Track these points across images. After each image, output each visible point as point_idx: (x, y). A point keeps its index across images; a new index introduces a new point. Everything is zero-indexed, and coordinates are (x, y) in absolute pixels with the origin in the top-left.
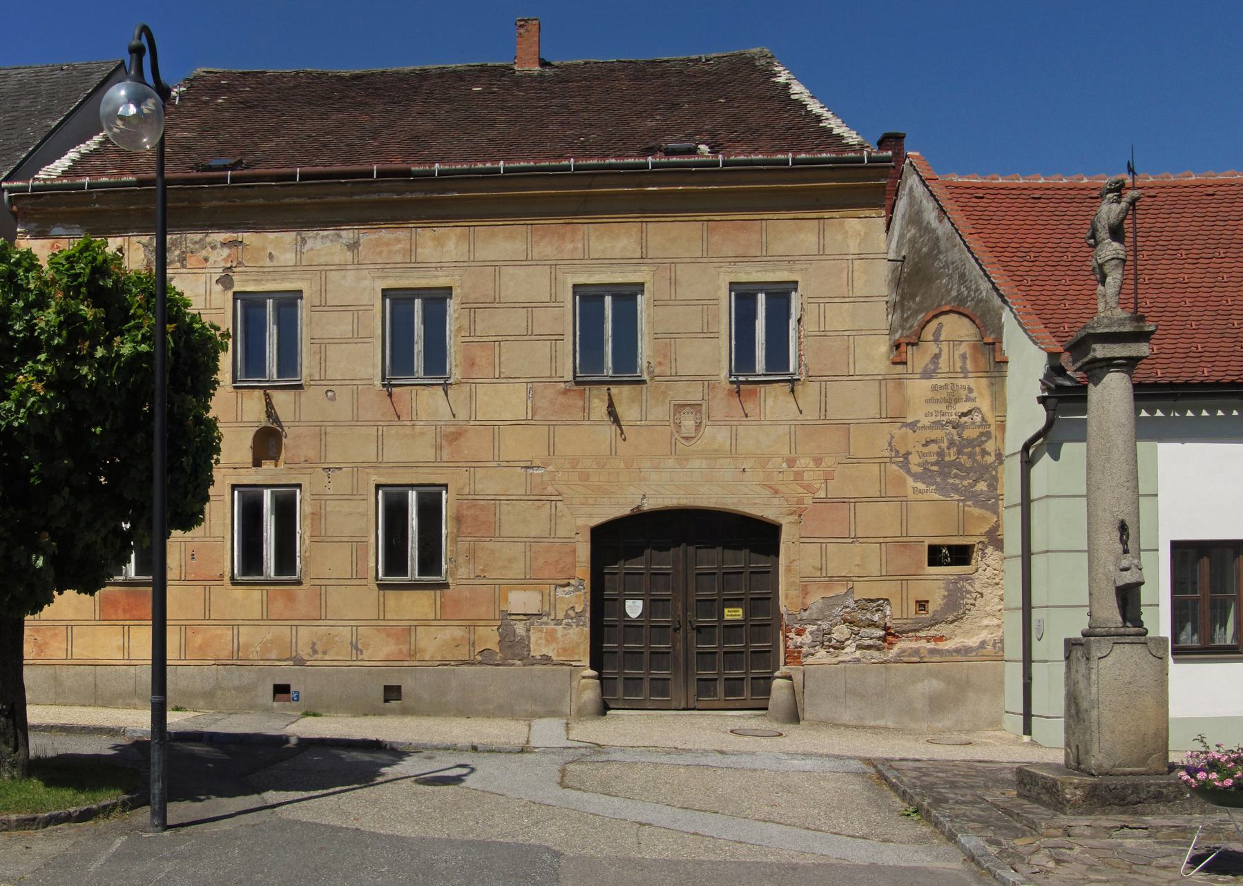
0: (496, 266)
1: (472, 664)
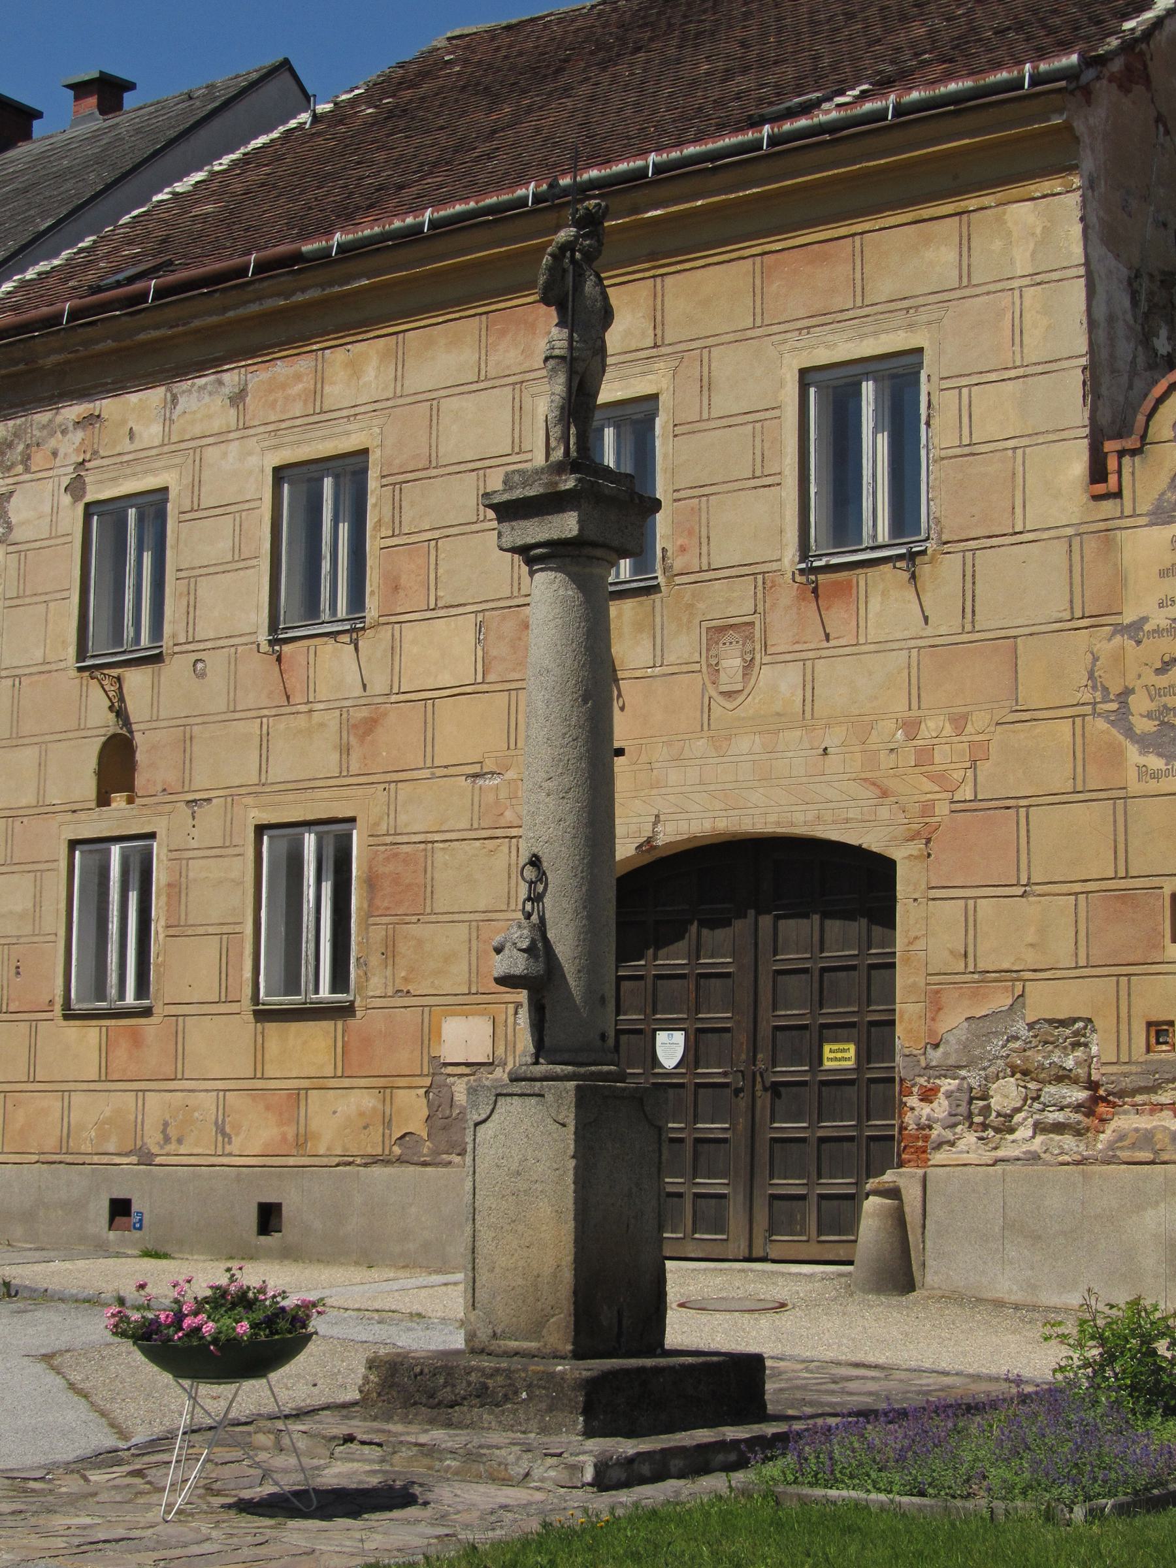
0: (432, 401)
1: (387, 1162)
